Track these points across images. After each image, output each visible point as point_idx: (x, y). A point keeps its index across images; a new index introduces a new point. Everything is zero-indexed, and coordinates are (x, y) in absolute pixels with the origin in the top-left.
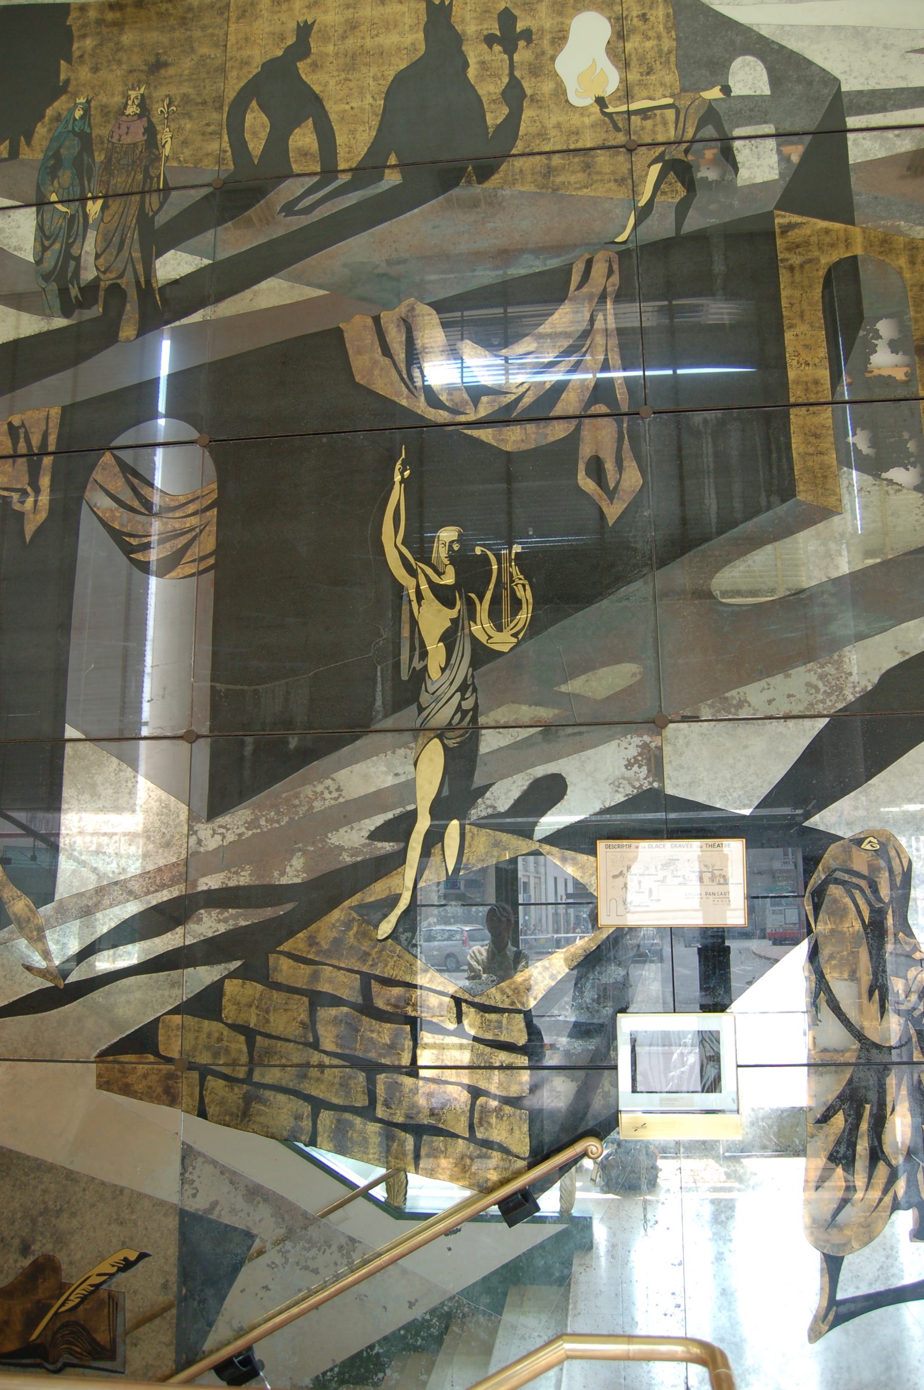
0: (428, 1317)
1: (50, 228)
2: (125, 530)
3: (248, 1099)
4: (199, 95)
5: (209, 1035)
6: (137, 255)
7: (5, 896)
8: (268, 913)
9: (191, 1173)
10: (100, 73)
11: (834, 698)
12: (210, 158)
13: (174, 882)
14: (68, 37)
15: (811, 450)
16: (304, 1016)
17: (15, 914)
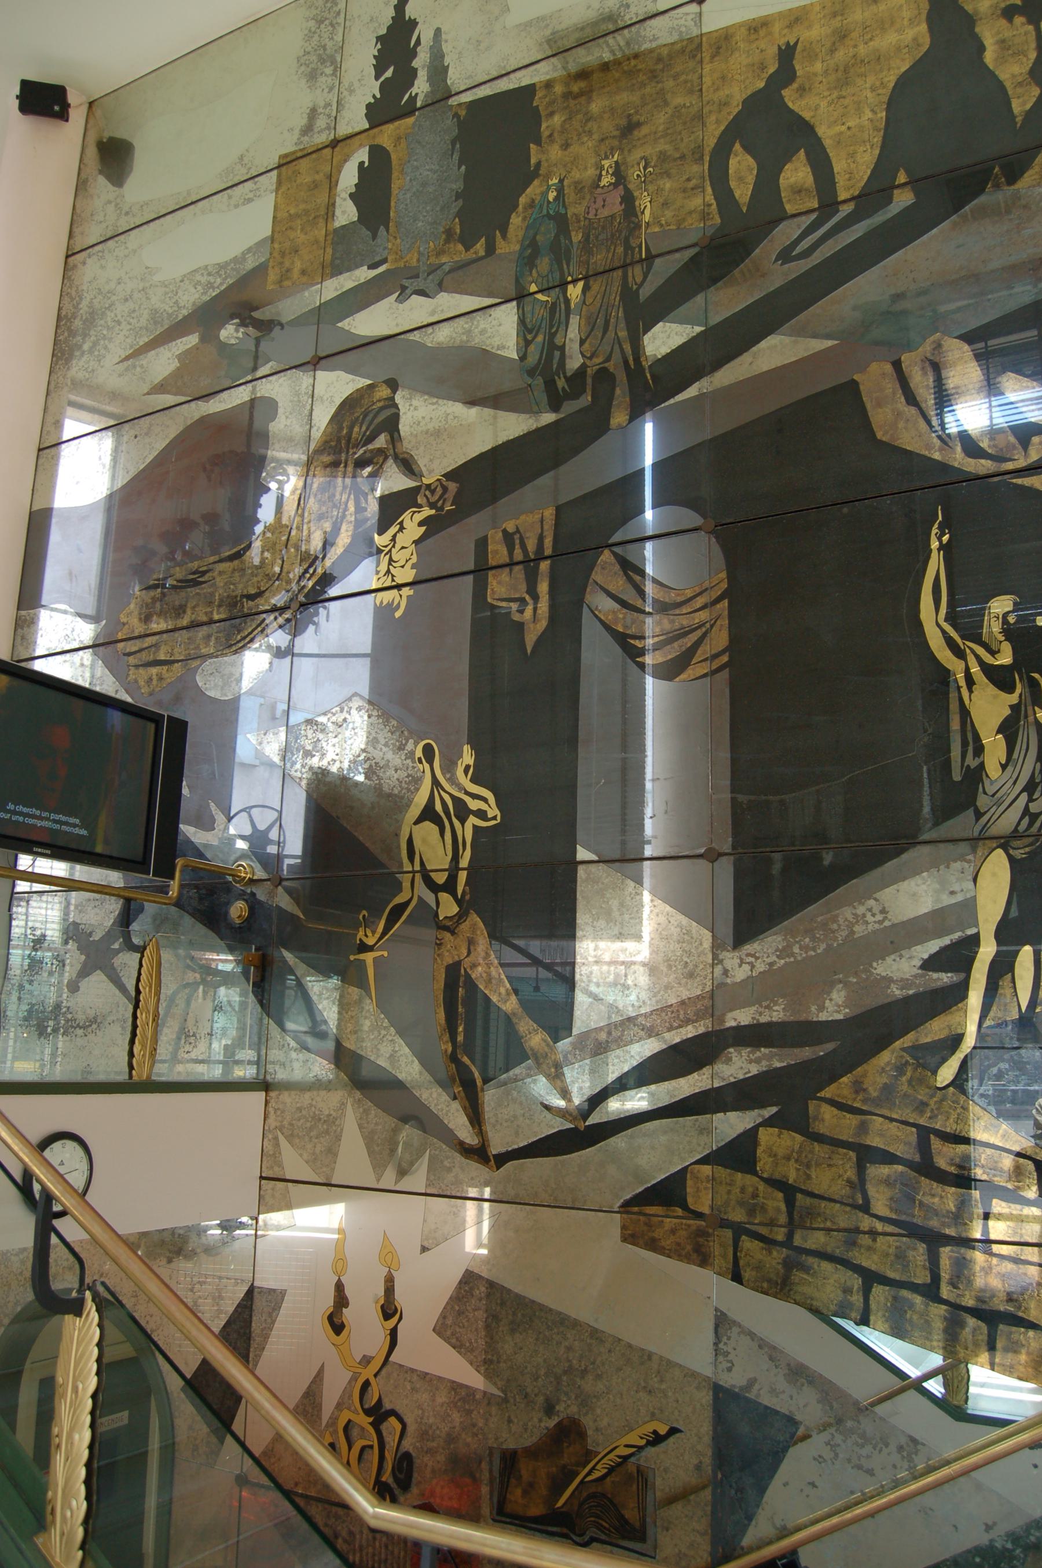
0: (1009, 1546)
1: (531, 321)
2: (629, 632)
3: (789, 1265)
4: (677, 149)
5: (743, 1190)
6: (623, 334)
7: (521, 1029)
8: (806, 1053)
9: (725, 1344)
10: (571, 149)
12: (694, 216)
13: (698, 1017)
14: (536, 118)
16: (851, 1173)
17: (532, 1049)
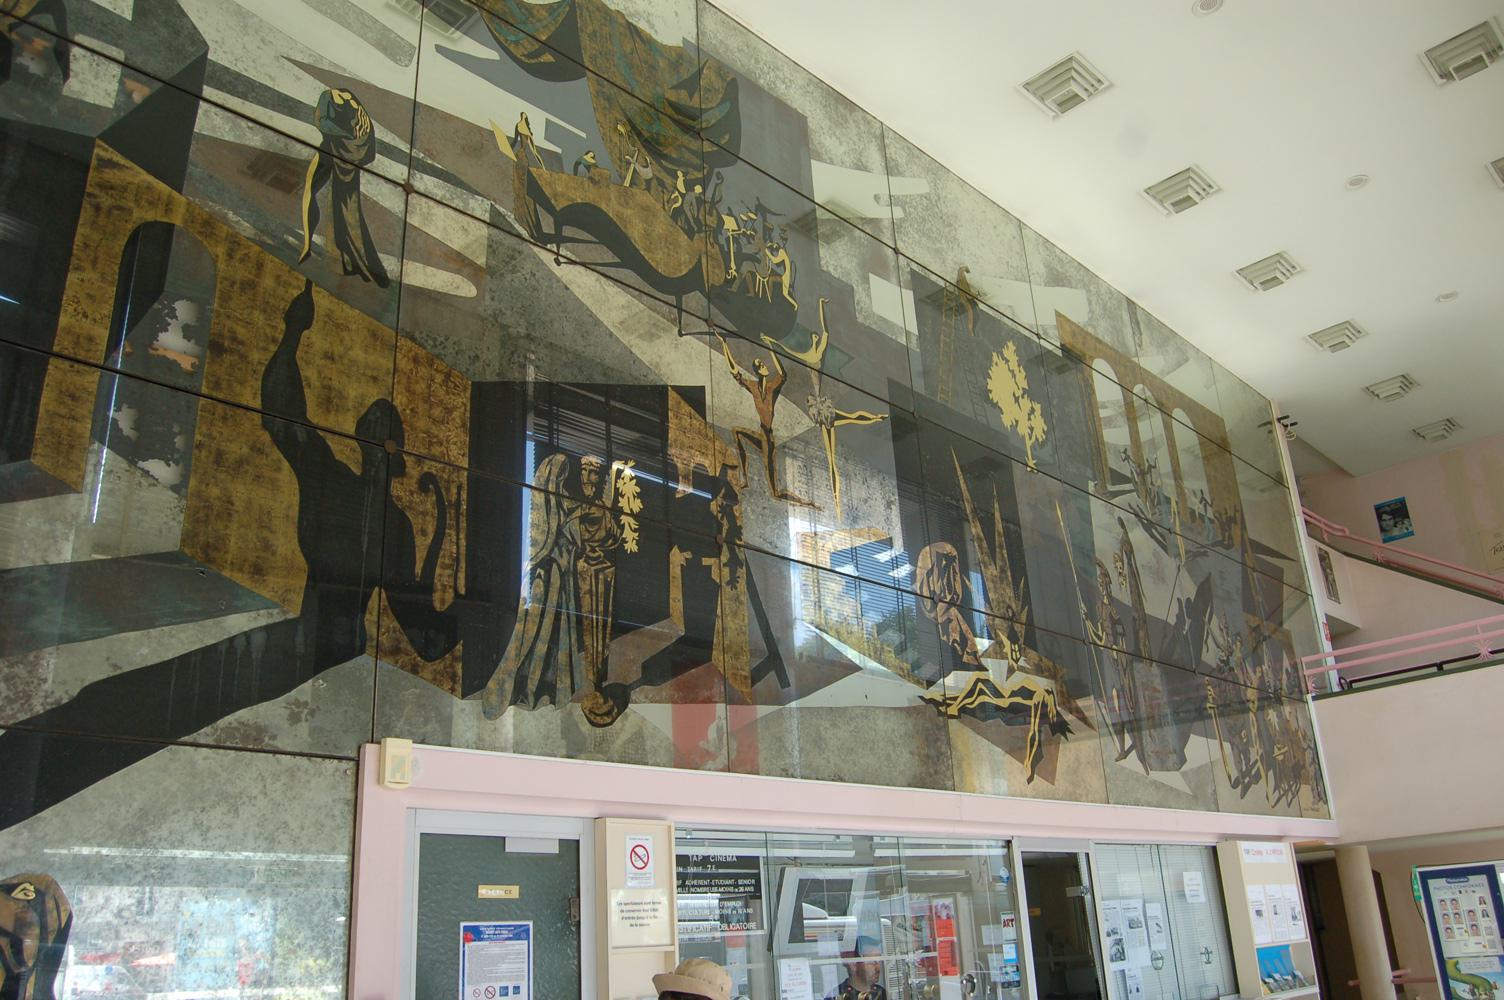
11: (16, 706)
15: (63, 411)
